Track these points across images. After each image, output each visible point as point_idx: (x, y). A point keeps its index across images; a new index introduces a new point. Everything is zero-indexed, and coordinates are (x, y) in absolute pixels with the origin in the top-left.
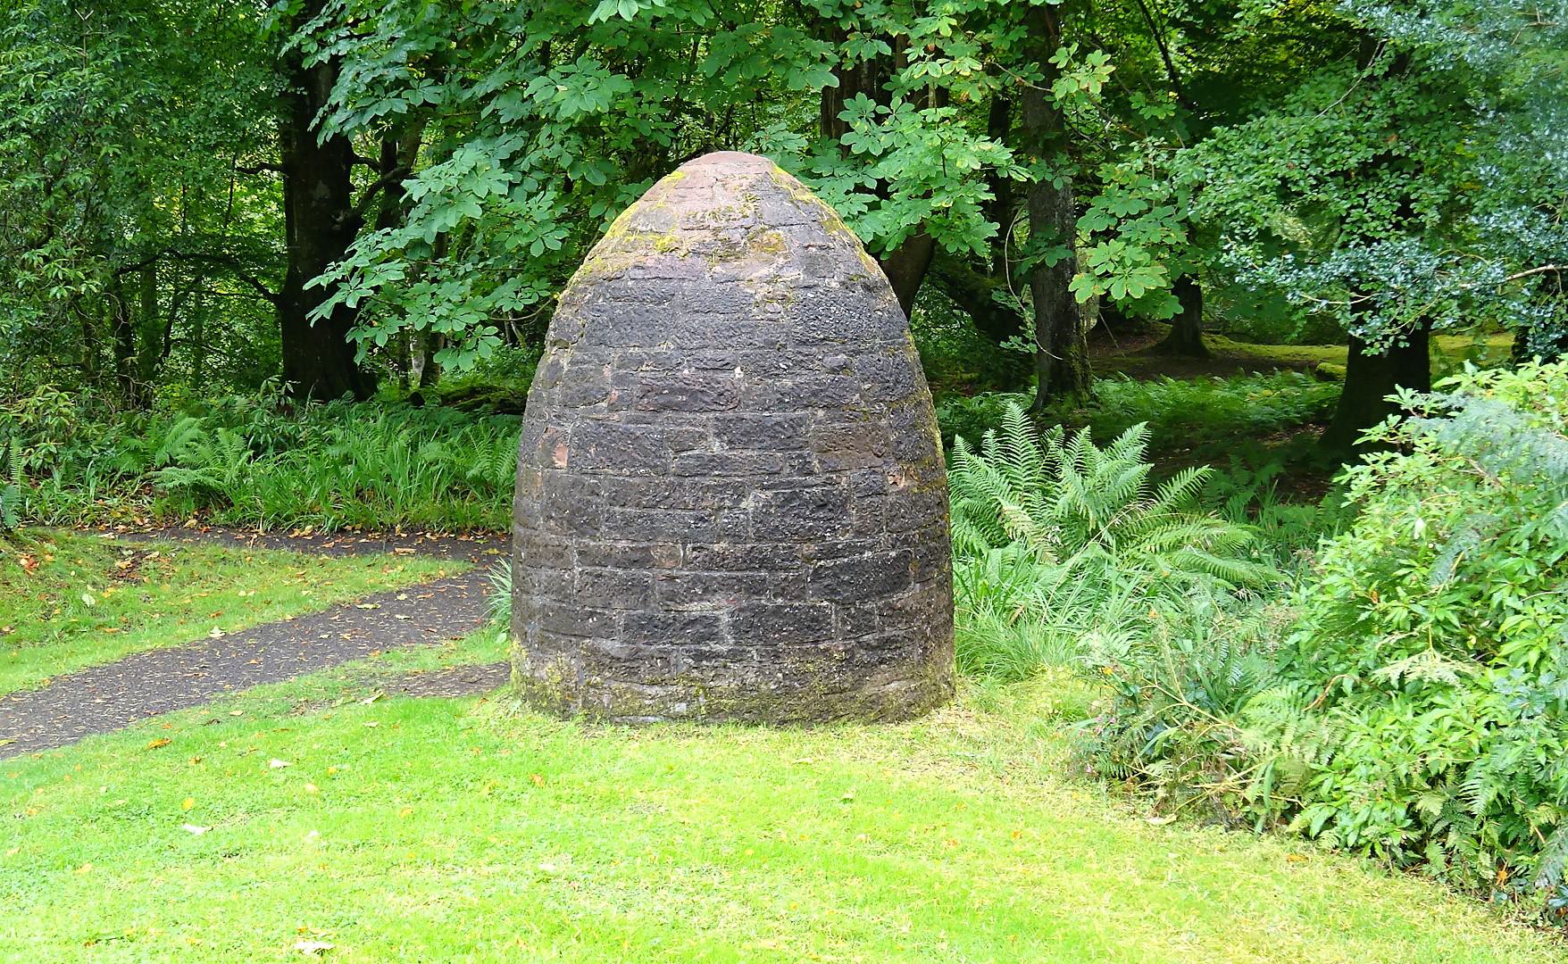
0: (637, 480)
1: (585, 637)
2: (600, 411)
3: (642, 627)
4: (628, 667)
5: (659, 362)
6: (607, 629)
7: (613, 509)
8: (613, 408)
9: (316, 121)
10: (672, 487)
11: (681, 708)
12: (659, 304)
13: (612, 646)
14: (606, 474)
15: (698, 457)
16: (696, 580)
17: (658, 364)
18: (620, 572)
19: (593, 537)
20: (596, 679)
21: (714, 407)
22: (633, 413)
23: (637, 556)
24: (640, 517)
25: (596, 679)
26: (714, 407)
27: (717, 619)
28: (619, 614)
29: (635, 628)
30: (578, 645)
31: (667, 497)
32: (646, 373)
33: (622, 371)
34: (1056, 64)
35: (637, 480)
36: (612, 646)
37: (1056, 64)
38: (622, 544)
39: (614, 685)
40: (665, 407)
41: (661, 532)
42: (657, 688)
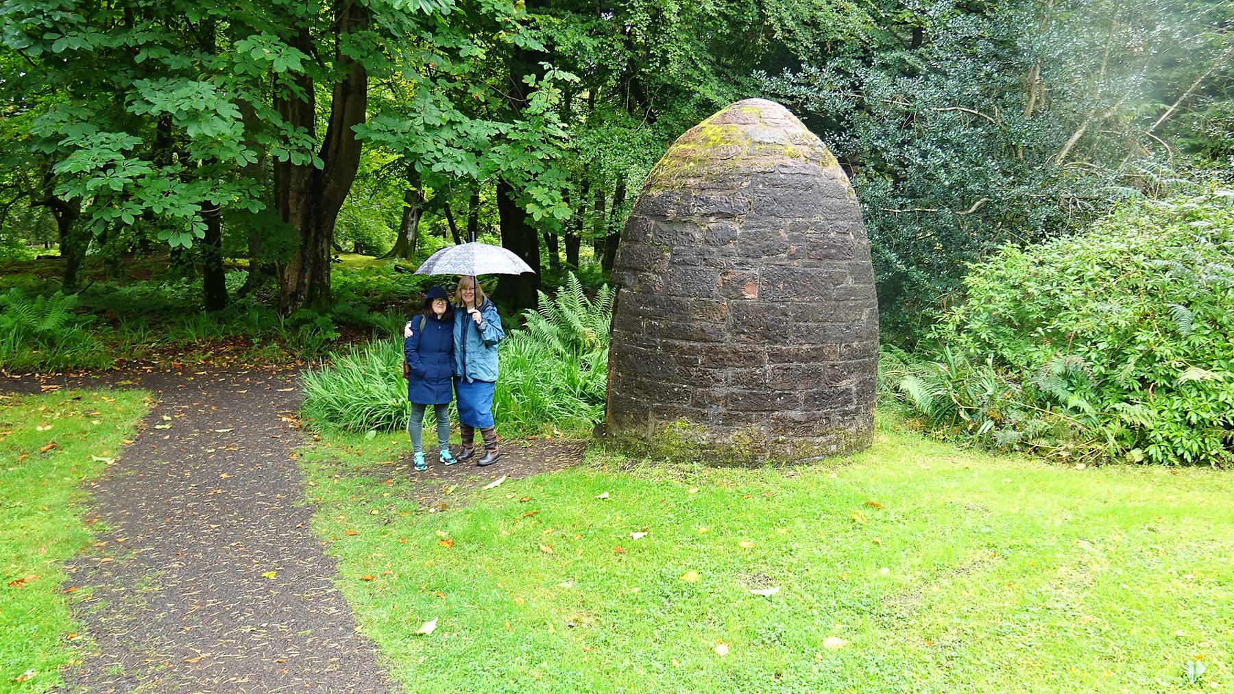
0: (814, 304)
1: (773, 411)
2: (781, 260)
3: (816, 399)
4: (806, 427)
5: (818, 228)
6: (792, 403)
7: (798, 324)
8: (792, 257)
9: (460, 366)
10: (835, 308)
11: (834, 448)
12: (806, 190)
13: (796, 414)
14: (793, 301)
15: (845, 288)
16: (846, 367)
17: (817, 229)
18: (803, 365)
19: (784, 344)
20: (781, 438)
21: (848, 257)
22: (807, 261)
23: (815, 354)
24: (817, 328)
25: (781, 438)
26: (848, 257)
27: (851, 389)
28: (800, 395)
29: (812, 401)
30: (768, 416)
31: (832, 315)
32: (811, 234)
33: (795, 234)
34: (535, 306)
35: (814, 304)
36: (796, 414)
37: (535, 306)
38: (805, 347)
39: (795, 440)
40: (826, 257)
41: (829, 337)
42: (821, 437)
